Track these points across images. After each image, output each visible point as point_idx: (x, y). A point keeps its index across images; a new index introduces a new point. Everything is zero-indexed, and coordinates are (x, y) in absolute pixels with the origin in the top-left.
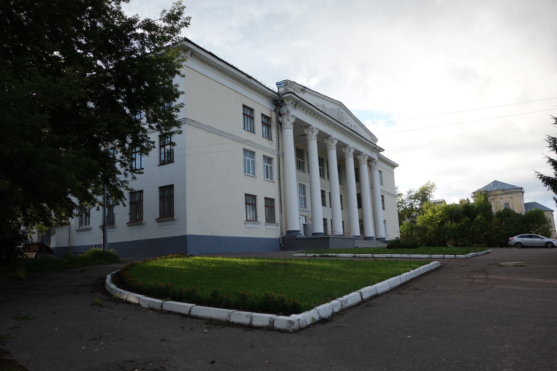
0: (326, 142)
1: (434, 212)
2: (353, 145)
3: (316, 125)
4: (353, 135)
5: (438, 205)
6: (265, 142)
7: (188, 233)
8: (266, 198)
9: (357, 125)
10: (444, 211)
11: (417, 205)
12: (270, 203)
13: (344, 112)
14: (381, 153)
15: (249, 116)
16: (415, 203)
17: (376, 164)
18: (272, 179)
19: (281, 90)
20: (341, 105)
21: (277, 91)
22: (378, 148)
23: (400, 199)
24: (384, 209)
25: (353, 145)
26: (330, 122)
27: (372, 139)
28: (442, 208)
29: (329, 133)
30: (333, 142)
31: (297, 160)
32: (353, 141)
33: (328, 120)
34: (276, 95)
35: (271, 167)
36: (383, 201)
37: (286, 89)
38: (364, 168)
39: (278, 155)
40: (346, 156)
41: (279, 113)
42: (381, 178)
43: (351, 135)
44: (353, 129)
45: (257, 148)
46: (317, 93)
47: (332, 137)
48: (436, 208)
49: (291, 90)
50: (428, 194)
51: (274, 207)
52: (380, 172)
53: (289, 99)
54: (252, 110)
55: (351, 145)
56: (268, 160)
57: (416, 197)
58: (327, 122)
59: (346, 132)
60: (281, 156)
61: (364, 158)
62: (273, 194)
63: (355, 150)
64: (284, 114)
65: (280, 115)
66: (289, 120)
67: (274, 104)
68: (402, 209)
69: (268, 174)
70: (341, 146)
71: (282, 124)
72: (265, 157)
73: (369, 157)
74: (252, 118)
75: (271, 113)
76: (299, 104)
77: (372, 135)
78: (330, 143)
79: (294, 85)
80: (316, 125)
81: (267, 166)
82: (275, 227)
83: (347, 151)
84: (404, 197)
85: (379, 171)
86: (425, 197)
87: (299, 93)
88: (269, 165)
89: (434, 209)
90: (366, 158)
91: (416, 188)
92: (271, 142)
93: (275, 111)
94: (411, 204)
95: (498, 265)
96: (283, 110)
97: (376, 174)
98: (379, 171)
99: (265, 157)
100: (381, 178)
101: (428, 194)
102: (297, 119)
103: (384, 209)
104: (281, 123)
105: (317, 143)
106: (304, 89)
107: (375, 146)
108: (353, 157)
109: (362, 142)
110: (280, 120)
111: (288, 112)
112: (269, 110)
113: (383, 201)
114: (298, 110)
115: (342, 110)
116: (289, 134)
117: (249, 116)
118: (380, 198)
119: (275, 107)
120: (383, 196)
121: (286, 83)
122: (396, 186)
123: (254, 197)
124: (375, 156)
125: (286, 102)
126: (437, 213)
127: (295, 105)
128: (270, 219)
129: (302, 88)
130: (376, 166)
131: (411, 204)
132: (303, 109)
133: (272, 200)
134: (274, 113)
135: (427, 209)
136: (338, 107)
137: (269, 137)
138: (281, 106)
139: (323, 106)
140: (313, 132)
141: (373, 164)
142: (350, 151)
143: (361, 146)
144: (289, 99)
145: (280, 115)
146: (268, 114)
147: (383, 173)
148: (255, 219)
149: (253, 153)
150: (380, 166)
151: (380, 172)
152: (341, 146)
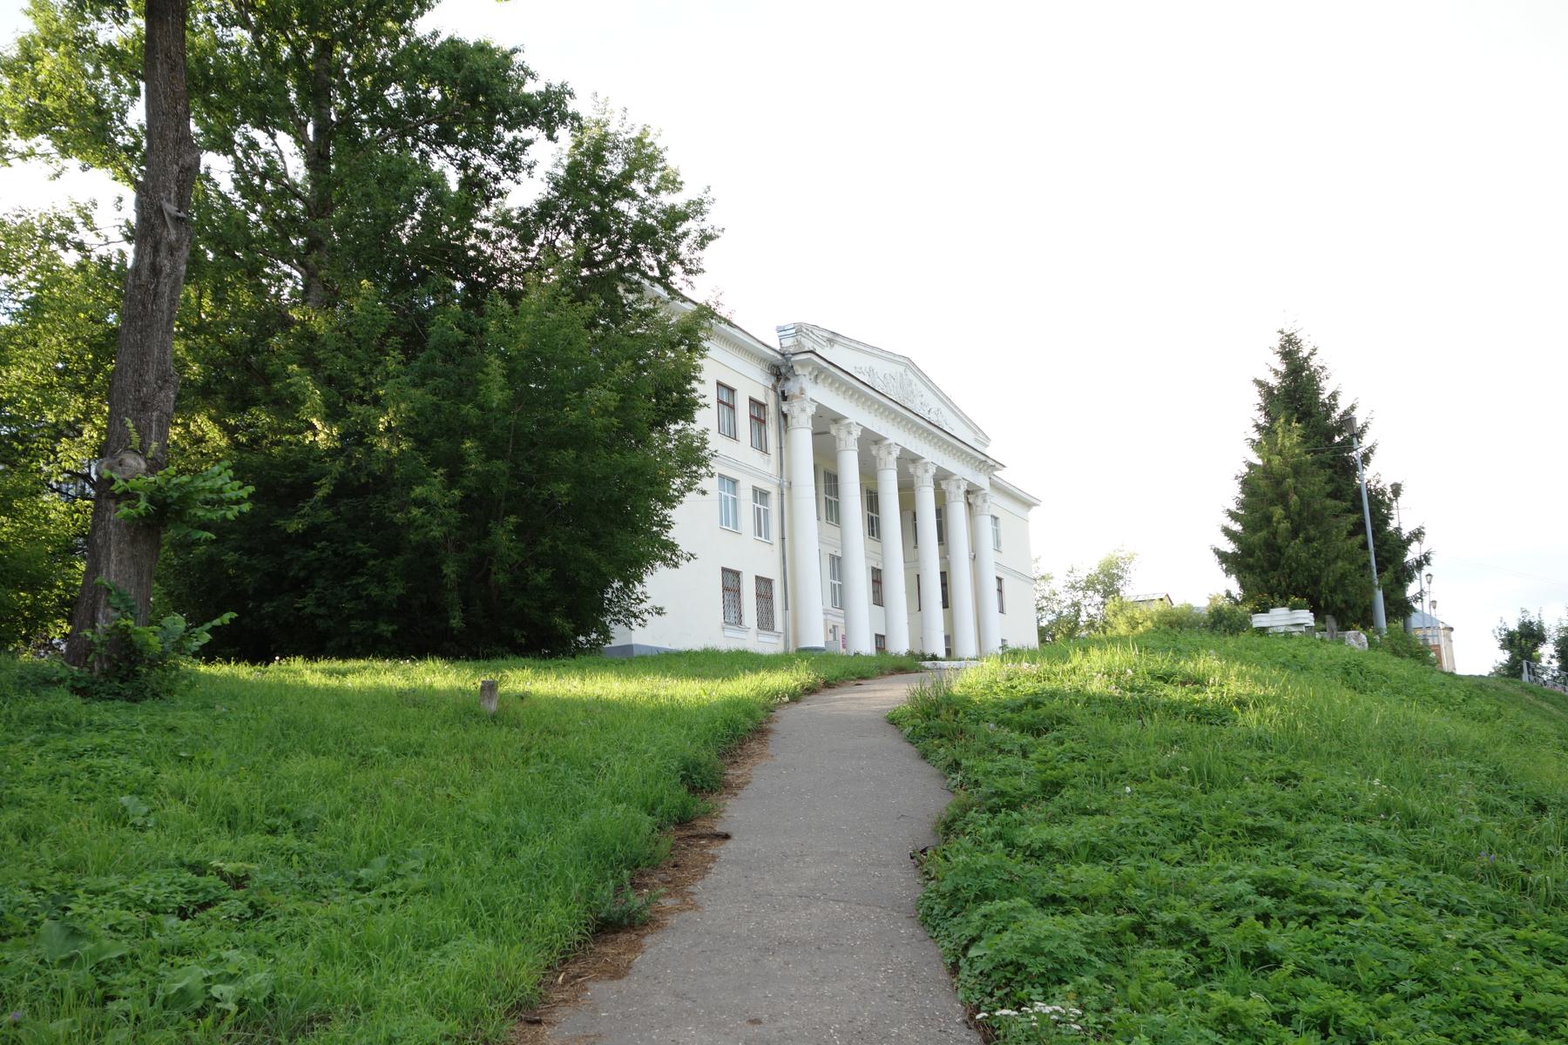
0: (874, 453)
1: (1133, 623)
2: (933, 456)
3: (857, 416)
4: (933, 433)
5: (1144, 607)
6: (755, 458)
7: (633, 642)
8: (757, 578)
9: (944, 410)
10: (1160, 621)
11: (1092, 605)
12: (764, 584)
13: (915, 380)
14: (996, 473)
15: (727, 405)
16: (1086, 602)
17: (985, 501)
18: (767, 537)
19: (788, 342)
20: (909, 364)
21: (778, 347)
22: (991, 463)
23: (1046, 589)
24: (1002, 611)
25: (933, 456)
26: (886, 408)
27: (976, 440)
28: (1153, 614)
29: (883, 433)
30: (890, 453)
31: (877, 513)
32: (912, 437)
33: (881, 405)
34: (779, 357)
35: (766, 511)
36: (1000, 591)
37: (799, 343)
38: (958, 511)
39: (780, 486)
40: (918, 483)
41: (783, 392)
42: (997, 533)
43: (930, 433)
44: (933, 418)
45: (742, 471)
46: (858, 343)
47: (847, 421)
48: (1137, 615)
49: (809, 345)
50: (1121, 578)
51: (771, 598)
52: (995, 518)
53: (803, 364)
54: (732, 391)
55: (891, 440)
56: (760, 495)
57: (1090, 585)
58: (847, 390)
59: (919, 427)
60: (787, 486)
61: (959, 487)
62: (772, 572)
63: (939, 468)
64: (794, 396)
65: (785, 398)
66: (803, 410)
67: (772, 374)
68: (1052, 617)
69: (761, 528)
70: (907, 460)
71: (789, 418)
72: (755, 490)
73: (970, 484)
74: (732, 408)
75: (766, 395)
76: (826, 372)
77: (977, 430)
78: (883, 453)
79: (815, 332)
80: (857, 416)
81: (759, 509)
82: (774, 640)
83: (920, 472)
84: (1058, 584)
85: (993, 516)
86: (1112, 585)
87: (822, 347)
88: (762, 507)
89: (1132, 618)
90: (964, 487)
91: (1089, 566)
92: (766, 456)
93: (774, 388)
94: (1076, 605)
95: (1144, 997)
96: (791, 387)
97: (986, 524)
98: (993, 516)
99: (755, 490)
100: (997, 533)
101: (1121, 578)
102: (820, 407)
103: (1002, 611)
104: (785, 416)
105: (814, 434)
106: (833, 338)
107: (983, 458)
108: (810, 425)
109: (867, 400)
110: (785, 409)
111: (802, 391)
112: (762, 389)
113: (1000, 591)
114: (820, 385)
115: (911, 376)
116: (803, 440)
117: (727, 405)
118: (994, 585)
119: (773, 379)
120: (999, 580)
121: (799, 330)
122: (1034, 555)
123: (737, 574)
124: (982, 481)
125: (798, 370)
126: (1141, 628)
127: (816, 377)
128: (766, 622)
129: (830, 336)
130: (986, 505)
131: (1076, 605)
132: (831, 384)
133: (769, 582)
134: (772, 394)
135: (1115, 615)
136: (901, 369)
137: (762, 446)
138: (787, 379)
139: (871, 370)
140: (850, 433)
141: (979, 502)
142: (926, 471)
143: (841, 396)
144: (803, 364)
145: (785, 398)
146: (761, 398)
147: (1001, 522)
148: (739, 621)
149: (734, 482)
150: (995, 504)
151: (995, 518)
152: (870, 441)
